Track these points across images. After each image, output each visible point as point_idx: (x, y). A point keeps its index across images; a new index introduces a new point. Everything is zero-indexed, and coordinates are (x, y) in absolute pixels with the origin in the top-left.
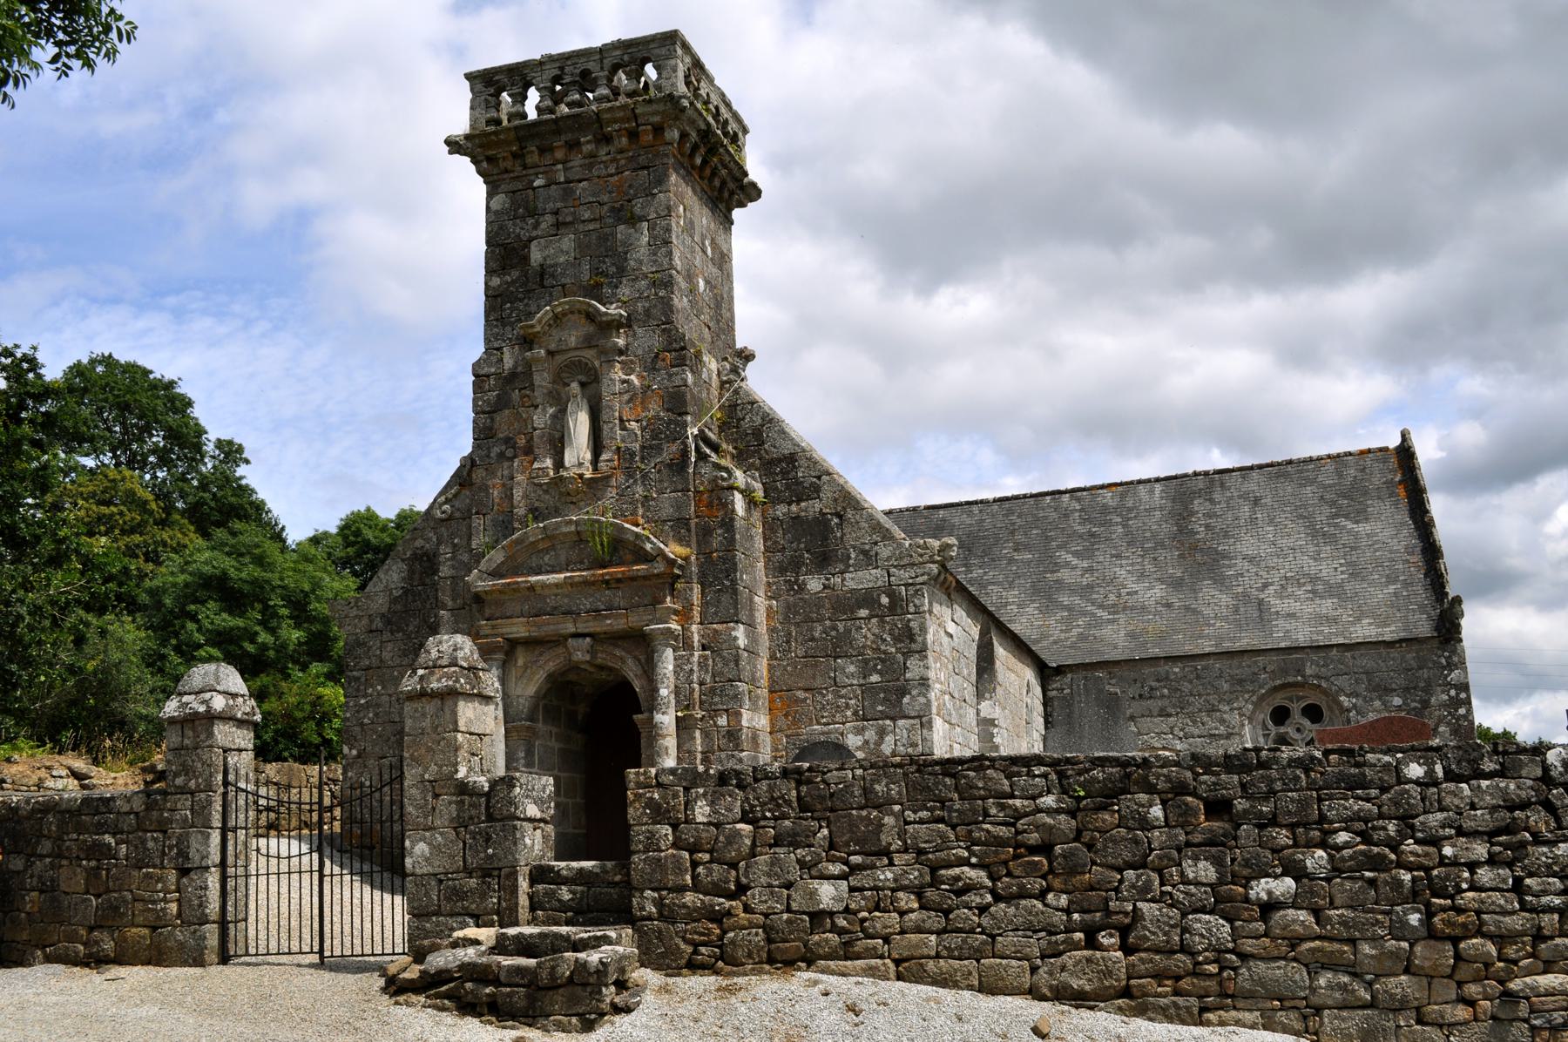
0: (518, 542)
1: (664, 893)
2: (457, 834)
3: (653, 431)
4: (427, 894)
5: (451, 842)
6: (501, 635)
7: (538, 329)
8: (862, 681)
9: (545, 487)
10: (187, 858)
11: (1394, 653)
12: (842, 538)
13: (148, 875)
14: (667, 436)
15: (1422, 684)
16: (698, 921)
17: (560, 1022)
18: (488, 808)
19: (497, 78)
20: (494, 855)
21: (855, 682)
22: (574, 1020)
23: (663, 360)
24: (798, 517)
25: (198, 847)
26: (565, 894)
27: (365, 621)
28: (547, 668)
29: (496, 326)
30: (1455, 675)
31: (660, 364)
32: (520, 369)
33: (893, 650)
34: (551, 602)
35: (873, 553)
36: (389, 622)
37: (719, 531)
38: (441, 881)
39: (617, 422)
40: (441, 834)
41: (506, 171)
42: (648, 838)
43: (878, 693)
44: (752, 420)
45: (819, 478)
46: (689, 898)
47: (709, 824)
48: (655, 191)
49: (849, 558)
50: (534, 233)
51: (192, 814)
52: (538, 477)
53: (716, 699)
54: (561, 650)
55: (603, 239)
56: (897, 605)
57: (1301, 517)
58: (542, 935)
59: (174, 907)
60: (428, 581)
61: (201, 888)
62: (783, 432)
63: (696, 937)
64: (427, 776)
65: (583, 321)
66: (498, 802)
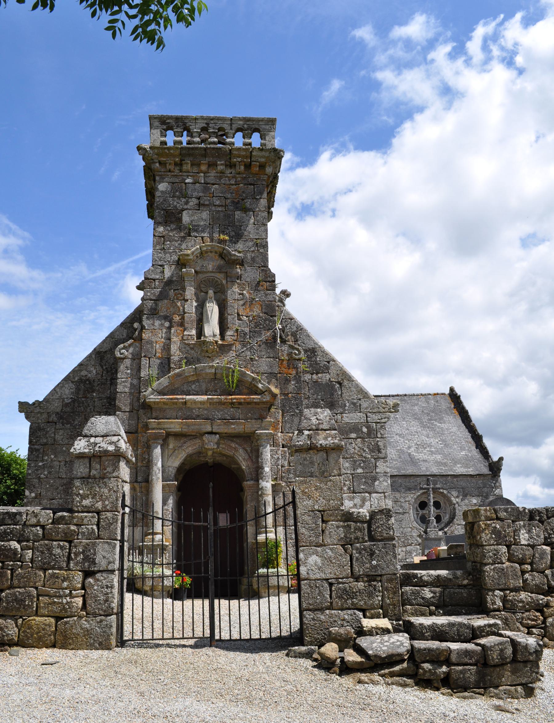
0: (178, 375)
1: (508, 592)
2: (346, 550)
3: (256, 323)
4: (320, 594)
5: (341, 555)
6: (164, 429)
7: (191, 257)
8: (352, 472)
9: (192, 346)
10: (94, 563)
11: (474, 480)
12: (341, 395)
13: (53, 576)
14: (264, 327)
15: (485, 495)
16: (529, 611)
17: (509, 691)
18: (370, 531)
19: (168, 121)
20: (378, 565)
21: (349, 472)
22: (519, 688)
23: (262, 286)
24: (317, 382)
25: (104, 554)
26: (427, 593)
27: (45, 416)
28: (187, 451)
29: (160, 253)
30: (497, 491)
31: (260, 288)
32: (174, 279)
33: (370, 456)
34: (196, 412)
35: (358, 404)
36: (61, 418)
37: (293, 383)
38: (331, 585)
39: (236, 315)
40: (331, 549)
41: (170, 171)
42: (495, 555)
43: (362, 479)
44: (291, 328)
45: (328, 362)
46: (523, 595)
47: (528, 545)
48: (258, 197)
49: (345, 406)
50: (185, 207)
51: (98, 529)
52: (188, 339)
53: (291, 476)
54: (198, 441)
55: (227, 216)
56: (371, 433)
57: (416, 418)
58: (451, 625)
59: (79, 601)
60: (88, 395)
61: (107, 587)
62: (308, 336)
63: (529, 622)
64: (316, 507)
65: (217, 257)
66: (378, 527)
